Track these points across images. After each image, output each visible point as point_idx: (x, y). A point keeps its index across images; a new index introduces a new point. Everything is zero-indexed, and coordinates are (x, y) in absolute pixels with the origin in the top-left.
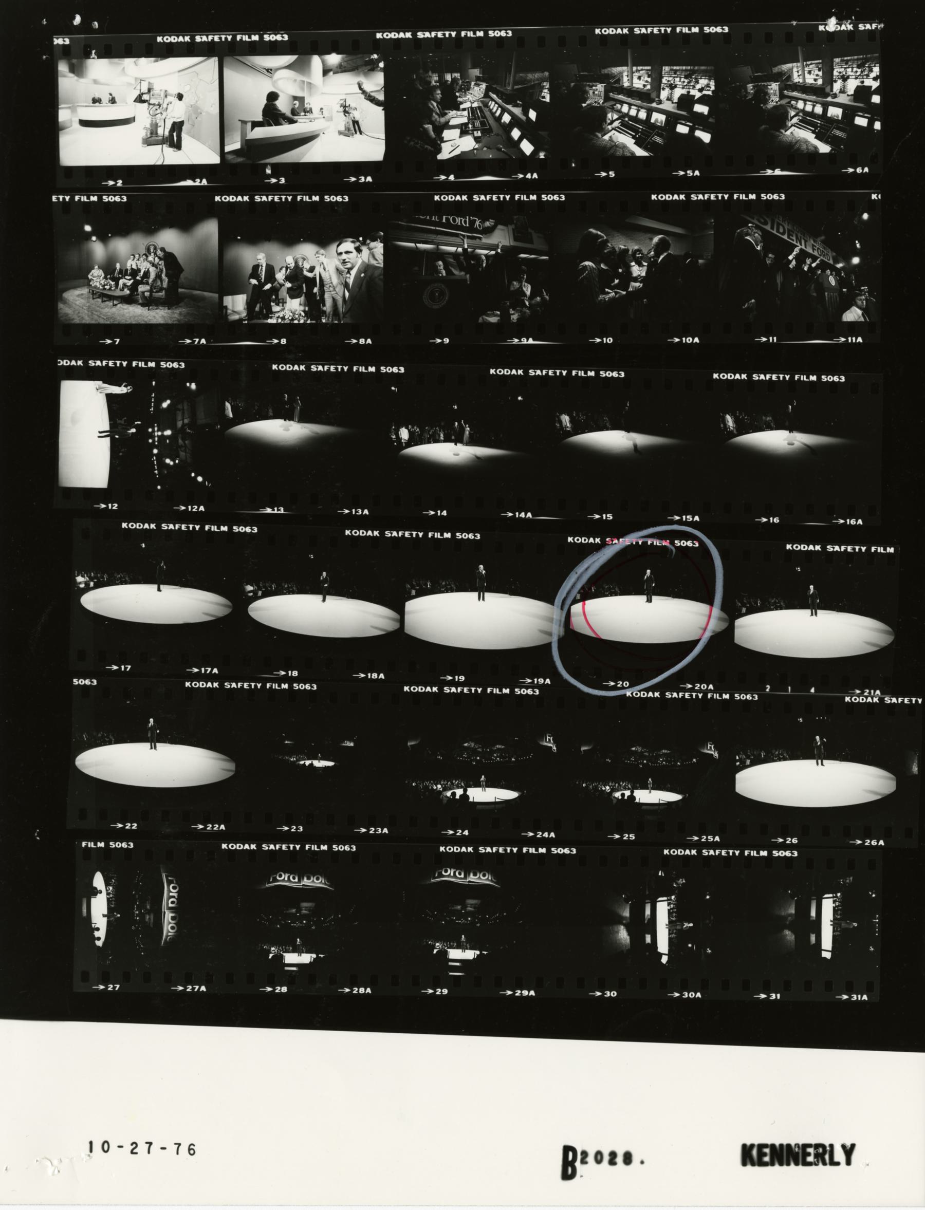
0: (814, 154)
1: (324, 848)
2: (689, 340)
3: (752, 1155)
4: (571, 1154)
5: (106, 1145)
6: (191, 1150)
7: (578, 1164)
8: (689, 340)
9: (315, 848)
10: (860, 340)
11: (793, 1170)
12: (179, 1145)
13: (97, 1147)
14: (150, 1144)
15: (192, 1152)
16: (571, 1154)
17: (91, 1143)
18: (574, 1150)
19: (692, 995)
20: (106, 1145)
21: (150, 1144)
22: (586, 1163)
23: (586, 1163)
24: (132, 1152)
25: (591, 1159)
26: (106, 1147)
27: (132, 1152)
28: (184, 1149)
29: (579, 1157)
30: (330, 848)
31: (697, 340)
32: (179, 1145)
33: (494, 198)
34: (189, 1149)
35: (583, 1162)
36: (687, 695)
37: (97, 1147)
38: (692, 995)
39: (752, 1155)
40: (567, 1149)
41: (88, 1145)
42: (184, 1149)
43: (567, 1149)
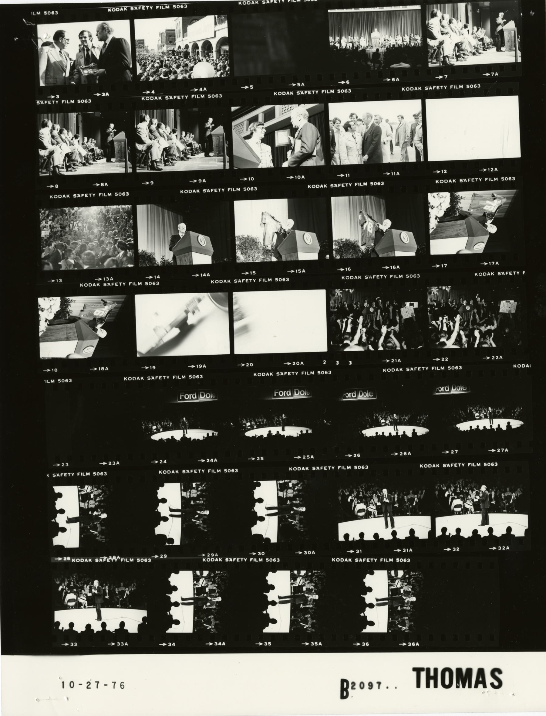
0: (474, 344)
1: (88, 474)
2: (299, 177)
3: (63, 687)
4: (345, 684)
5: (72, 684)
6: (122, 686)
7: (350, 690)
8: (299, 177)
9: (83, 474)
10: (398, 174)
11: (457, 693)
12: (115, 683)
13: (67, 685)
14: (98, 682)
15: (122, 687)
16: (345, 684)
17: (63, 683)
18: (347, 681)
19: (309, 553)
20: (72, 684)
21: (98, 682)
22: (355, 689)
23: (355, 689)
24: (87, 688)
25: (357, 686)
26: (72, 684)
27: (87, 688)
28: (118, 685)
29: (350, 685)
30: (92, 474)
31: (303, 177)
32: (115, 683)
33: (455, 465)
34: (121, 685)
35: (353, 688)
36: (49, 102)
37: (67, 685)
38: (309, 553)
39: (63, 687)
40: (343, 681)
41: (62, 684)
42: (118, 685)
43: (343, 681)
